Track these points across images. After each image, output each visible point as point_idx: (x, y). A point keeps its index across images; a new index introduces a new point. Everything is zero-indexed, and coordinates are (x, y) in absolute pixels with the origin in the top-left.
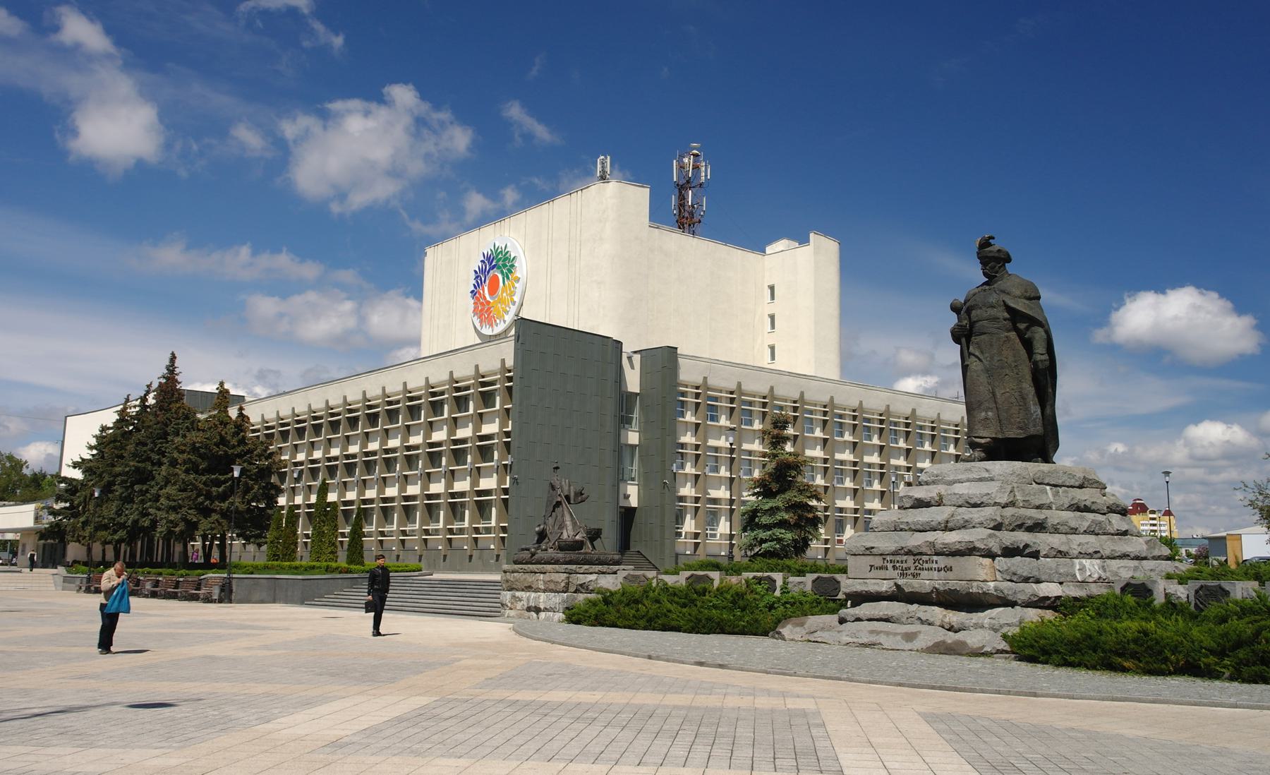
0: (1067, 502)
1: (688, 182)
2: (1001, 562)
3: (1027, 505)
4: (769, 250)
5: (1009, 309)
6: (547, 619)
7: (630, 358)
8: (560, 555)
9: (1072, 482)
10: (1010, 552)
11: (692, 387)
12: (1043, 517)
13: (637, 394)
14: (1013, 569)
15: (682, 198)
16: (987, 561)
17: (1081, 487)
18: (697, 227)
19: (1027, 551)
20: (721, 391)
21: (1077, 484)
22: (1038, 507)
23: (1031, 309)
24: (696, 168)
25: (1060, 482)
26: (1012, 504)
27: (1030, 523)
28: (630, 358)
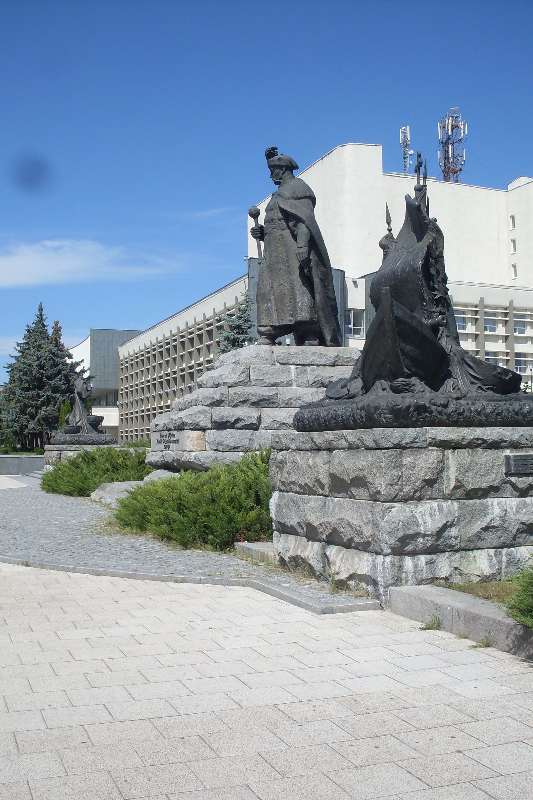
0: (312, 379)
1: (449, 139)
2: (212, 434)
3: (260, 383)
4: (510, 187)
5: (282, 211)
6: (338, 501)
7: (355, 283)
8: (68, 437)
9: (323, 361)
10: (220, 425)
11: (472, 306)
12: (272, 393)
13: (364, 310)
14: (218, 441)
15: (446, 152)
16: (196, 434)
17: (333, 365)
18: (461, 175)
19: (239, 425)
20: (526, 310)
21: (328, 363)
22: (273, 385)
23: (296, 207)
24: (455, 127)
25: (308, 362)
26: (246, 383)
27: (254, 399)
28: (355, 283)
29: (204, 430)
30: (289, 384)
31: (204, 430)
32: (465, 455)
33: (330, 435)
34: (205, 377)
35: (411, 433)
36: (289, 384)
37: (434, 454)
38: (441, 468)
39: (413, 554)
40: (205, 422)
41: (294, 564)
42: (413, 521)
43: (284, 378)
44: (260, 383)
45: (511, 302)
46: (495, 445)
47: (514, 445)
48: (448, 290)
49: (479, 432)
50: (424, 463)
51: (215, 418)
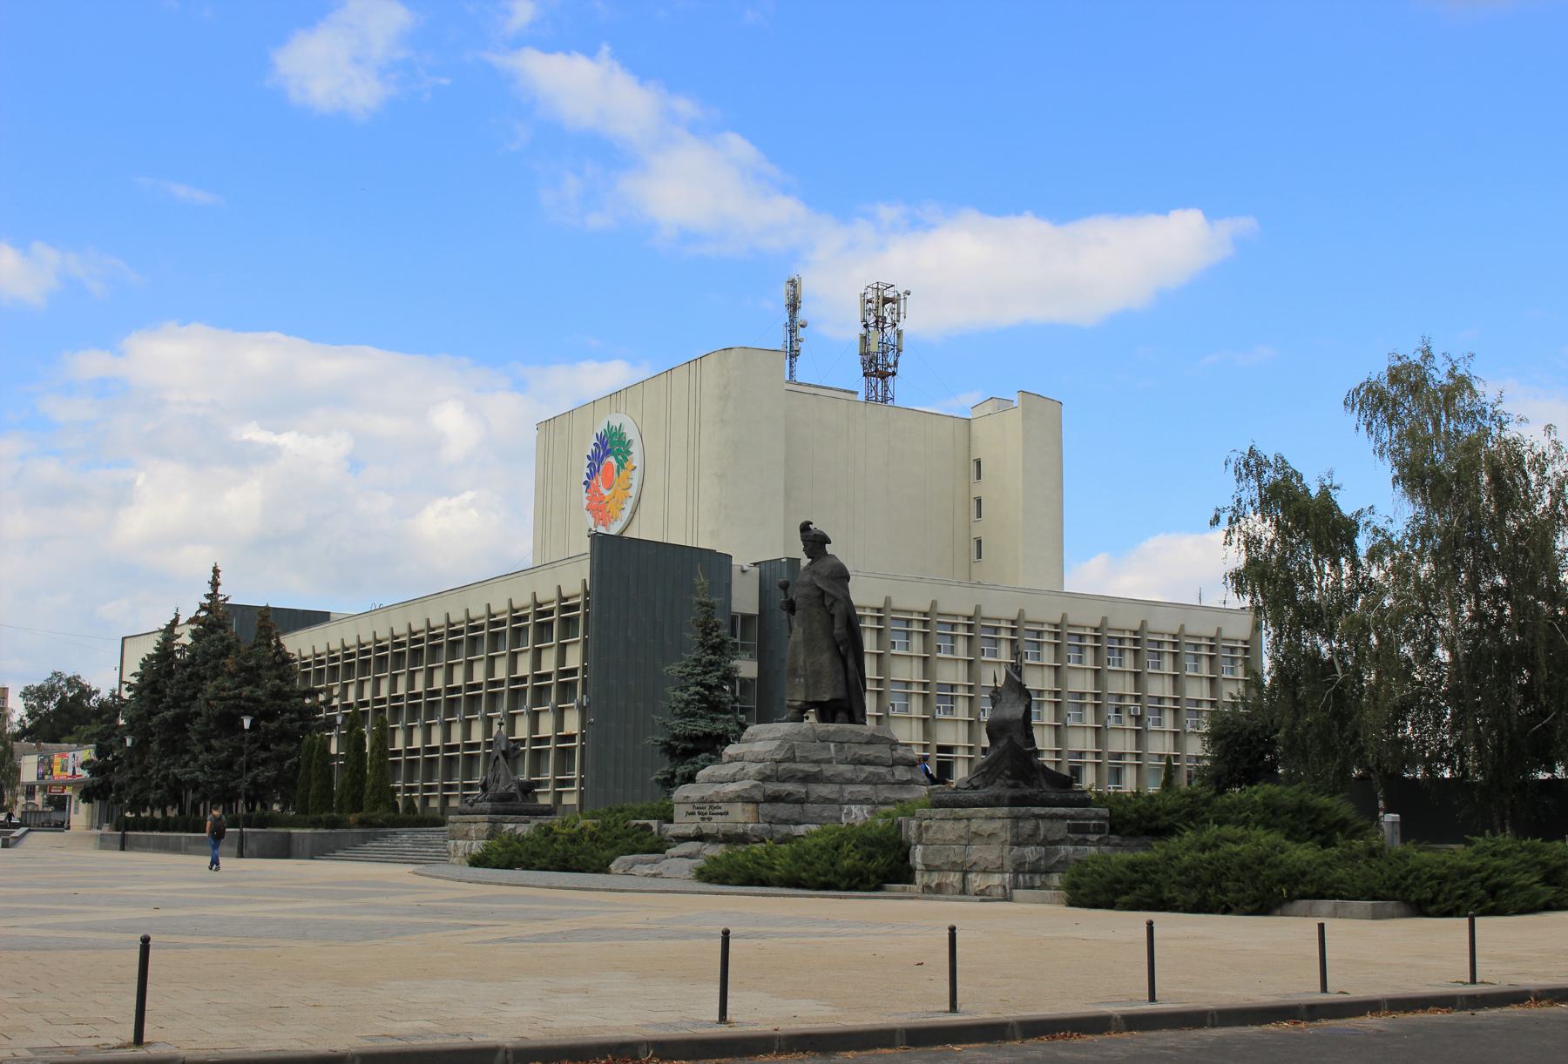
2: (766, 808)
10: (775, 799)
17: (869, 743)
26: (793, 759)
29: (757, 803)
30: (829, 761)
31: (757, 803)
32: (1048, 823)
33: (971, 811)
34: (731, 750)
35: (1023, 809)
36: (829, 761)
37: (1033, 822)
38: (1037, 828)
39: (1024, 873)
40: (758, 795)
41: (927, 888)
42: (1023, 856)
43: (825, 755)
44: (805, 760)
45: (978, 608)
46: (1063, 817)
47: (1072, 818)
48: (826, 540)
49: (1055, 810)
50: (1027, 827)
51: (769, 792)
